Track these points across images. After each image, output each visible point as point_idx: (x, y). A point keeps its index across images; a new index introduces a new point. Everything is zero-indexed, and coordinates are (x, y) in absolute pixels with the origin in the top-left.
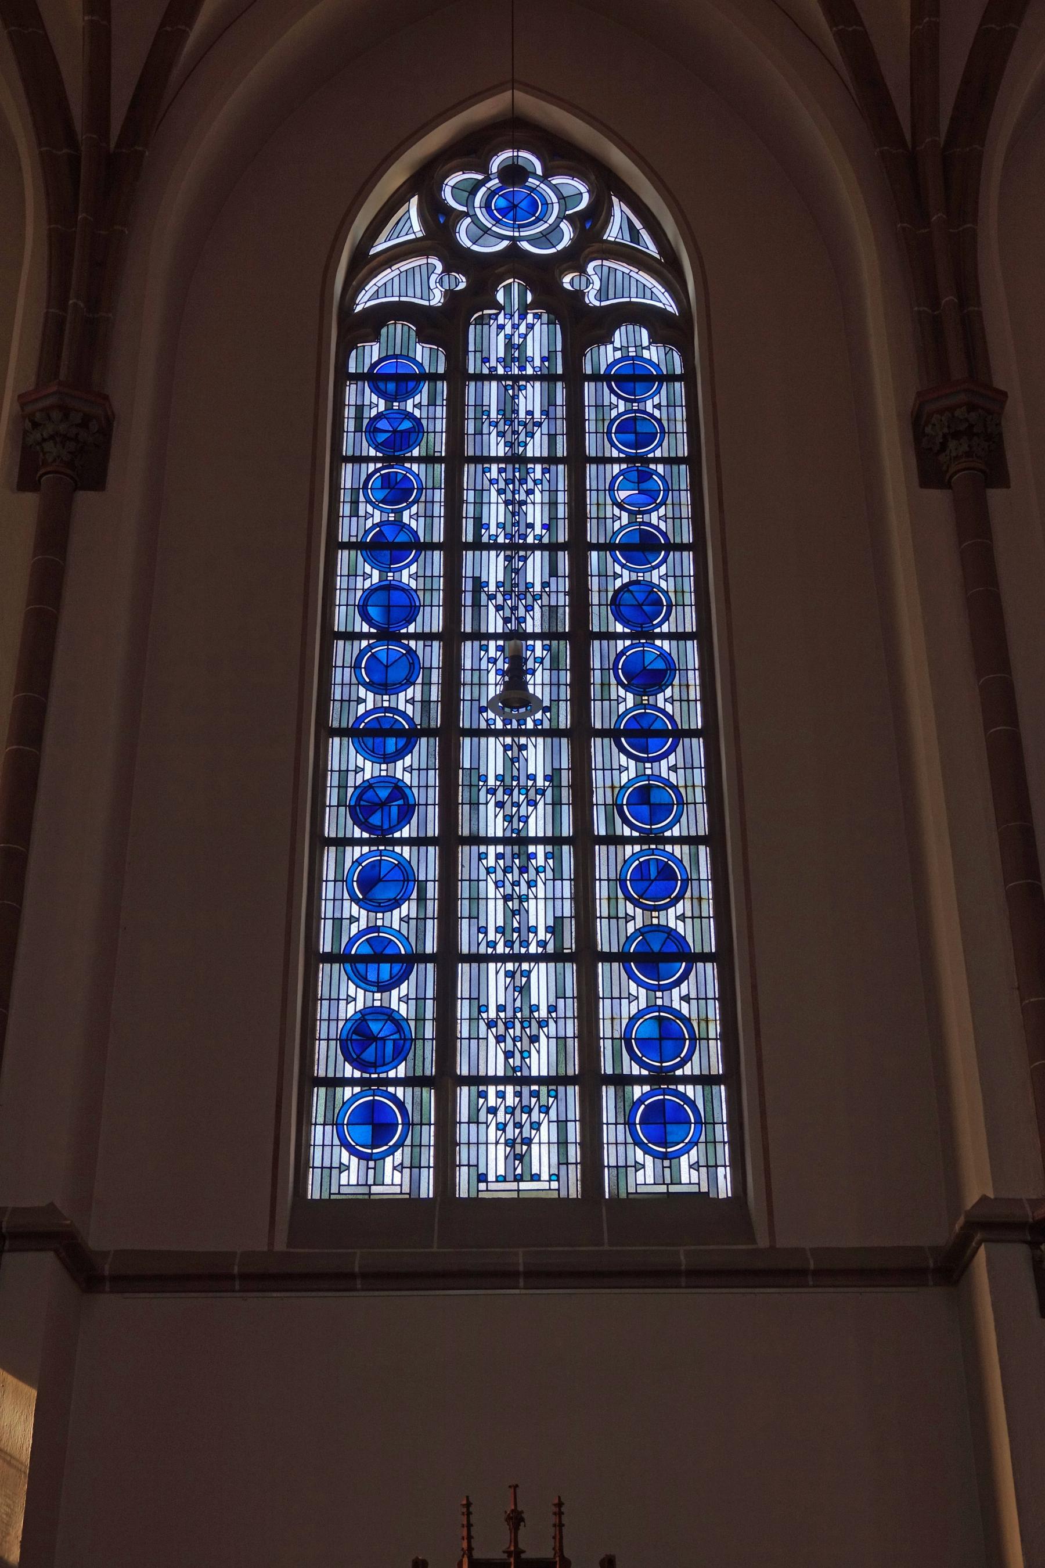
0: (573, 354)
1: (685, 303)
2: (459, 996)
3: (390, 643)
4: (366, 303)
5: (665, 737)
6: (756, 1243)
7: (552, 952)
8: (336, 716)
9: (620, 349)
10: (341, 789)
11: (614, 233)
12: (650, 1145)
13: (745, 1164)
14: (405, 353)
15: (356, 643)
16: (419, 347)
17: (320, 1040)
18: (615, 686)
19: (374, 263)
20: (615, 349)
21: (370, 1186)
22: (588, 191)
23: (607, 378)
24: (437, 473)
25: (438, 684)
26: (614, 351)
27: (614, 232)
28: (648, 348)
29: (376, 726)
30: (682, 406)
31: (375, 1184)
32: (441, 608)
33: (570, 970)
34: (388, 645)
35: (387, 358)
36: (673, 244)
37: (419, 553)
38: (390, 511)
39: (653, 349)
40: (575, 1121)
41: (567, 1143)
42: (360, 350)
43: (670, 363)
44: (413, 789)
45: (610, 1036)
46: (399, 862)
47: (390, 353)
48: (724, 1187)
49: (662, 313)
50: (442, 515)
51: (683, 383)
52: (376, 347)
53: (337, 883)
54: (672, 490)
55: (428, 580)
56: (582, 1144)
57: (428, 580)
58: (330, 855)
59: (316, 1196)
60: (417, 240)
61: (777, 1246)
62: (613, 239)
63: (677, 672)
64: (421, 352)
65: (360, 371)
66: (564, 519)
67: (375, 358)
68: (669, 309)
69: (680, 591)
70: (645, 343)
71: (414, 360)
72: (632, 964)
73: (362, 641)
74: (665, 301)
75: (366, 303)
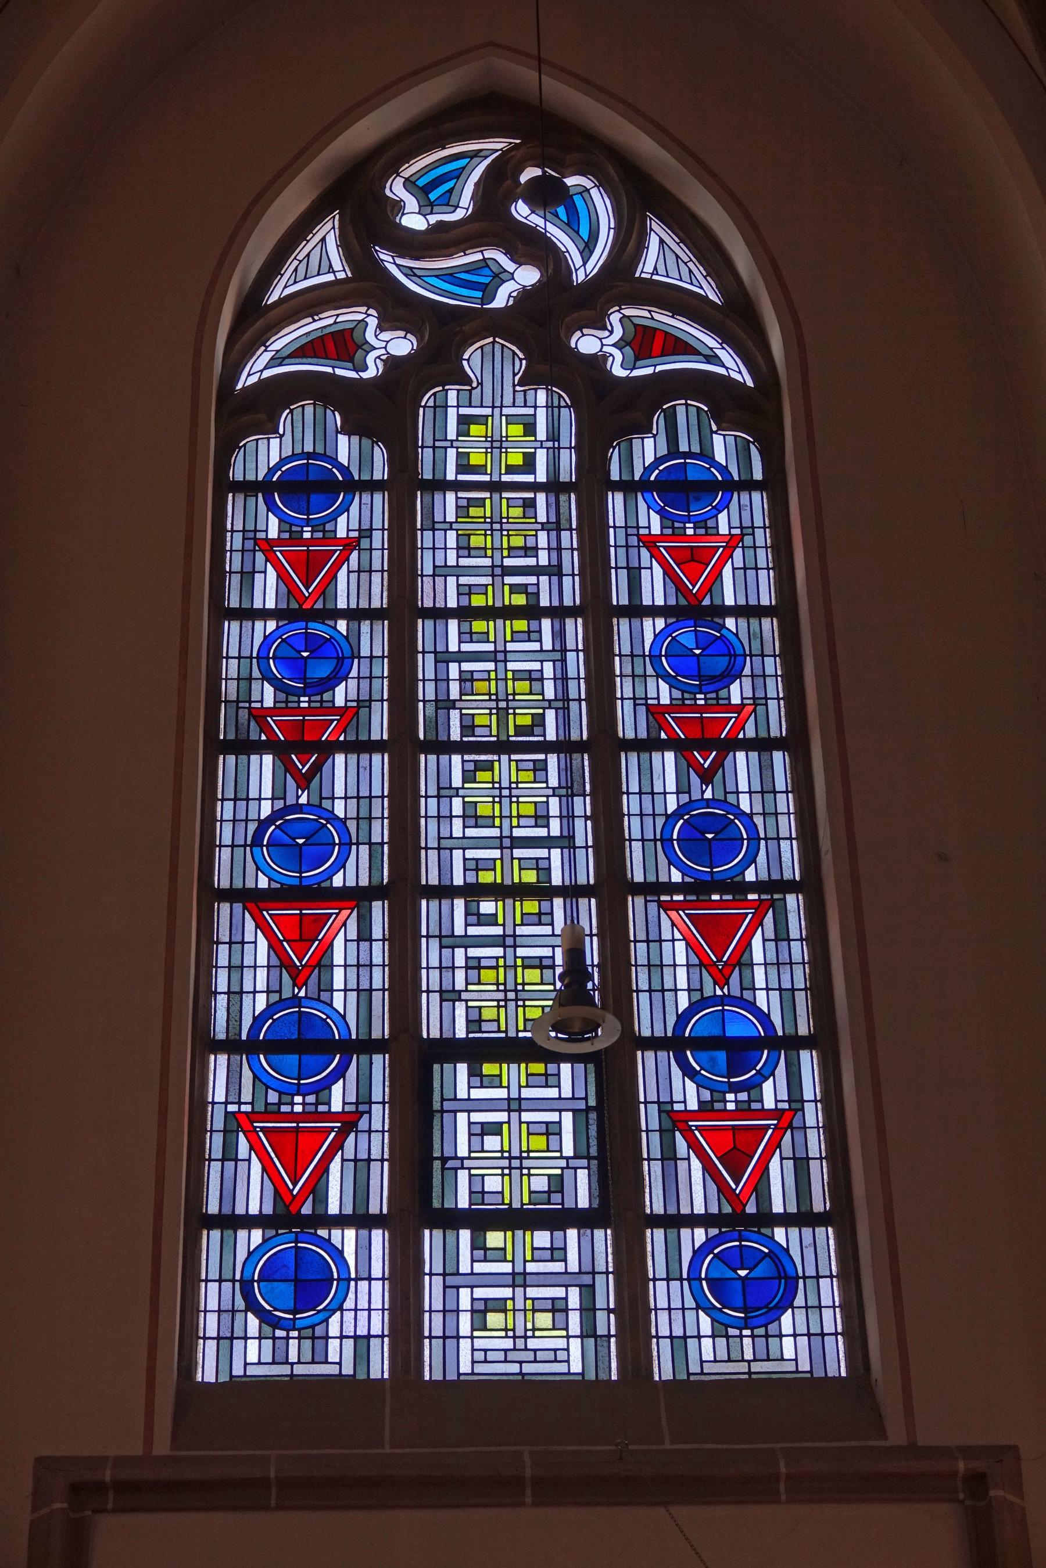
1: (764, 368)
2: (420, 649)
4: (262, 371)
6: (886, 1439)
10: (239, 963)
11: (649, 268)
13: (867, 1342)
14: (320, 450)
15: (259, 625)
16: (343, 440)
17: (207, 1281)
19: (272, 315)
21: (292, 1364)
23: (643, 486)
25: (383, 1310)
27: (649, 264)
29: (301, 477)
31: (299, 1362)
32: (386, 1282)
34: (301, 877)
35: (294, 457)
37: (349, 497)
38: (305, 809)
44: (348, 822)
45: (668, 1334)
46: (332, 637)
47: (298, 450)
48: (838, 1365)
49: (726, 382)
52: (275, 443)
54: (751, 656)
55: (364, 803)
56: (578, 449)
57: (364, 803)
58: (212, 1239)
60: (337, 282)
61: (920, 1443)
62: (649, 276)
63: (748, 658)
64: (344, 448)
71: (334, 461)
73: (268, 623)
75: (262, 371)
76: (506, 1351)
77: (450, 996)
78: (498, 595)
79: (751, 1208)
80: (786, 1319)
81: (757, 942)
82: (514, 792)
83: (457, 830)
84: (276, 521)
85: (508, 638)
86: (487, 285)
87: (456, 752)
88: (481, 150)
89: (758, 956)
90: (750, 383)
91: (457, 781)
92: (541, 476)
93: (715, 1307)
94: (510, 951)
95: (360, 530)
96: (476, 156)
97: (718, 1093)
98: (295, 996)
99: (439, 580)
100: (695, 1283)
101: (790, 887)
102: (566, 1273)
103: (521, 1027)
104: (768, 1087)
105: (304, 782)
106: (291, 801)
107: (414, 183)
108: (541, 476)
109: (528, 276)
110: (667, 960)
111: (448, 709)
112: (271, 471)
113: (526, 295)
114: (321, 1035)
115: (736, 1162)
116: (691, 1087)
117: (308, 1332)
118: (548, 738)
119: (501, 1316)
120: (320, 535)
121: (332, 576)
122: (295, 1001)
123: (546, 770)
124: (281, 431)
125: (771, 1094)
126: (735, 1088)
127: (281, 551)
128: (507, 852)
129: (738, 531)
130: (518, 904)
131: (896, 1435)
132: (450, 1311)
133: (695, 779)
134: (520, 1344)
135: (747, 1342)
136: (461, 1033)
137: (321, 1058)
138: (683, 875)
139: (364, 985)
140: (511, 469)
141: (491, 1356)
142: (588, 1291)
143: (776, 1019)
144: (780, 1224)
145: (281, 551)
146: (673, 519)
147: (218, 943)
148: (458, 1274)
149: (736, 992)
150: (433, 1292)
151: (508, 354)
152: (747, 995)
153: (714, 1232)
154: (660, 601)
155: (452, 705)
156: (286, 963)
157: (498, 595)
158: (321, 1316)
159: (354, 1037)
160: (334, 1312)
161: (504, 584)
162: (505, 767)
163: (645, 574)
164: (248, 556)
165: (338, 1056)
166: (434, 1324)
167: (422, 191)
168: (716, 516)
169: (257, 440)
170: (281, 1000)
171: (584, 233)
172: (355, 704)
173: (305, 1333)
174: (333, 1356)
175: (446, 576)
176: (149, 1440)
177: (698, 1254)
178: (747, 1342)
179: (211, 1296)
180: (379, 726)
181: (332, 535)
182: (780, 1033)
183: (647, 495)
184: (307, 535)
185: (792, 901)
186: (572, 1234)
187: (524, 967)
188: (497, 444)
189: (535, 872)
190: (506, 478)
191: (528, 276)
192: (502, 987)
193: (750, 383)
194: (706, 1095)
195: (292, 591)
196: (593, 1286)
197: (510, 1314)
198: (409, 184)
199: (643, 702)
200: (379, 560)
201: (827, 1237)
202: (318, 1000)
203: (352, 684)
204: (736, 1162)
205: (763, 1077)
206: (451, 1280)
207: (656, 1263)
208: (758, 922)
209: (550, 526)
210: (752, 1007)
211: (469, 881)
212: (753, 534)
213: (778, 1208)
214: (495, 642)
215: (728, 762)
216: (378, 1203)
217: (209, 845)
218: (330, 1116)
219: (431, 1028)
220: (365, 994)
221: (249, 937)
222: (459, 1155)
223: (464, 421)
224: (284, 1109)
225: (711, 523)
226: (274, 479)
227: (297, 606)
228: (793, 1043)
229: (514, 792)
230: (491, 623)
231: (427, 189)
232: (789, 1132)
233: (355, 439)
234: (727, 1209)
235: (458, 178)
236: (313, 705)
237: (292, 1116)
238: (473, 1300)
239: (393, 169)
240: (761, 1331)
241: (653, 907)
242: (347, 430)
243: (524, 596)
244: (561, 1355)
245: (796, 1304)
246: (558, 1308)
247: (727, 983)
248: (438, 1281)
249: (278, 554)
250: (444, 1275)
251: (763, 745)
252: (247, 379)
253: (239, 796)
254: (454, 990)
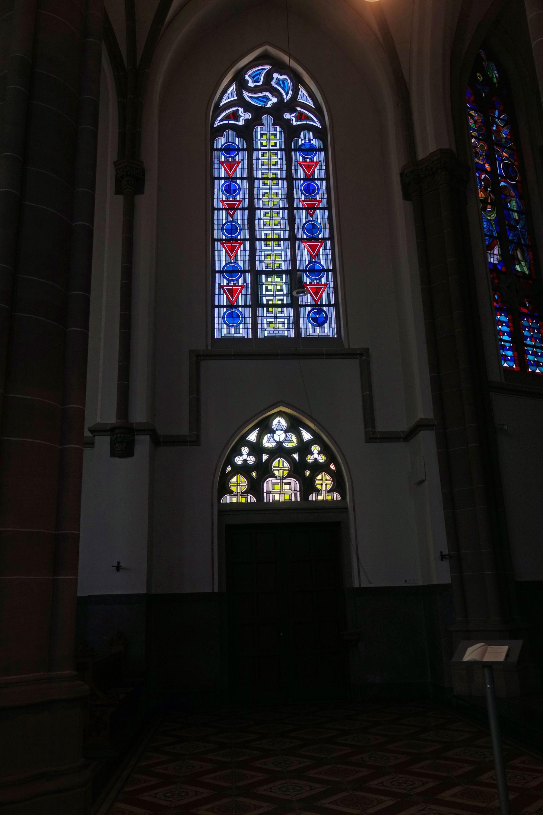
0: (288, 141)
3: (231, 238)
5: (312, 151)
7: (294, 501)
8: (216, 234)
9: (304, 140)
12: (306, 194)
14: (232, 141)
16: (237, 139)
18: (301, 195)
20: (302, 140)
22: (289, 78)
24: (245, 154)
26: (302, 141)
28: (312, 140)
30: (334, 317)
33: (289, 243)
35: (227, 143)
36: (319, 102)
37: (238, 152)
39: (314, 140)
40: (293, 328)
41: (290, 323)
42: (217, 140)
43: (319, 145)
50: (251, 328)
51: (329, 241)
52: (223, 139)
53: (218, 230)
59: (218, 338)
64: (237, 141)
65: (219, 270)
66: (292, 316)
67: (223, 143)
68: (319, 126)
69: (324, 224)
70: (312, 138)
71: (235, 144)
72: (307, 273)
74: (318, 124)
76: (273, 331)
77: (261, 262)
78: (270, 183)
79: (319, 303)
80: (326, 325)
81: (321, 250)
82: (275, 261)
83: (260, 167)
84: (224, 157)
85: (272, 185)
86: (266, 101)
87: (260, 151)
88: (265, 68)
89: (321, 253)
90: (321, 128)
91: (260, 157)
92: (278, 147)
93: (312, 323)
94: (272, 228)
95: (242, 199)
96: (263, 69)
97: (313, 281)
98: (231, 262)
99: (258, 171)
100: (303, 230)
101: (328, 239)
102: (281, 249)
103: (273, 206)
104: (323, 279)
105: (231, 216)
106: (229, 220)
107: (250, 76)
108: (278, 147)
109: (275, 100)
110: (304, 259)
111: (259, 160)
112: (222, 146)
113: (274, 104)
114: (236, 269)
115: (316, 293)
116: (308, 279)
117: (236, 328)
118: (280, 207)
119: (272, 325)
120: (233, 160)
121: (235, 170)
122: (231, 263)
123: (277, 154)
124: (224, 137)
125: (323, 281)
126: (316, 279)
127: (225, 164)
128: (273, 248)
129: (318, 161)
130: (272, 181)
131: (346, 346)
132: (263, 324)
133: (309, 216)
134: (276, 330)
135: (318, 329)
136: (264, 269)
137: (237, 274)
138: (307, 236)
139: (246, 325)
140: (272, 146)
141: (271, 332)
142: (288, 320)
143: (325, 266)
144: (317, 180)
145: (225, 164)
146: (307, 196)
147: (215, 189)
148: (259, 168)
149: (317, 261)
150: (259, 320)
151: (271, 119)
152: (319, 261)
153: (312, 308)
154: (302, 177)
155: (259, 159)
156: (229, 255)
157: (270, 183)
158: (238, 325)
159: (243, 269)
160: (241, 324)
161: (272, 212)
162: (268, 154)
163: (299, 170)
164: (218, 165)
165: (240, 273)
166: (260, 326)
167: (252, 77)
168: (314, 157)
169: (219, 139)
170: (228, 263)
171: (286, 90)
172: (241, 199)
173: (235, 328)
174: (241, 332)
175: (262, 252)
176: (207, 347)
177: (309, 312)
178: (318, 329)
179: (217, 321)
180: (246, 204)
181: (235, 160)
182: (325, 269)
183: (299, 152)
184: (230, 160)
185: (330, 274)
186: (285, 309)
187: (276, 255)
188: (269, 140)
189: (281, 311)
190: (271, 148)
191: (275, 100)
192: (280, 494)
193: (321, 128)
194: (311, 281)
195: (227, 173)
196: (289, 319)
197: (274, 324)
198: (250, 76)
199: (299, 199)
200: (246, 166)
201: (333, 309)
202: (236, 262)
203: (241, 195)
204: (316, 293)
205: (321, 277)
206: (262, 318)
207: (301, 315)
208: (321, 246)
209: (282, 200)
210: (320, 263)
211: (262, 177)
212: (321, 162)
213: (324, 303)
214: (274, 314)
215: (316, 212)
216: (249, 303)
217: (213, 229)
218: (239, 286)
219: (258, 268)
220: (245, 262)
221: (220, 167)
222: (270, 491)
223: (262, 135)
224: (229, 284)
225: (312, 159)
226: (223, 148)
227: (229, 176)
228: (327, 271)
229: (275, 261)
230: (271, 242)
231: (254, 77)
232: (326, 288)
233: (240, 139)
234: (314, 303)
235: (260, 75)
236: (233, 199)
237: (231, 286)
238: (267, 321)
239: (246, 73)
240: (321, 327)
241: (301, 242)
242: (238, 137)
243: (275, 175)
244: (283, 332)
245: (327, 322)
246: (283, 323)
247: (315, 259)
248: (260, 318)
249: (224, 164)
250: (261, 317)
251: (323, 209)
252: (216, 125)
253: (218, 229)
254: (262, 260)
